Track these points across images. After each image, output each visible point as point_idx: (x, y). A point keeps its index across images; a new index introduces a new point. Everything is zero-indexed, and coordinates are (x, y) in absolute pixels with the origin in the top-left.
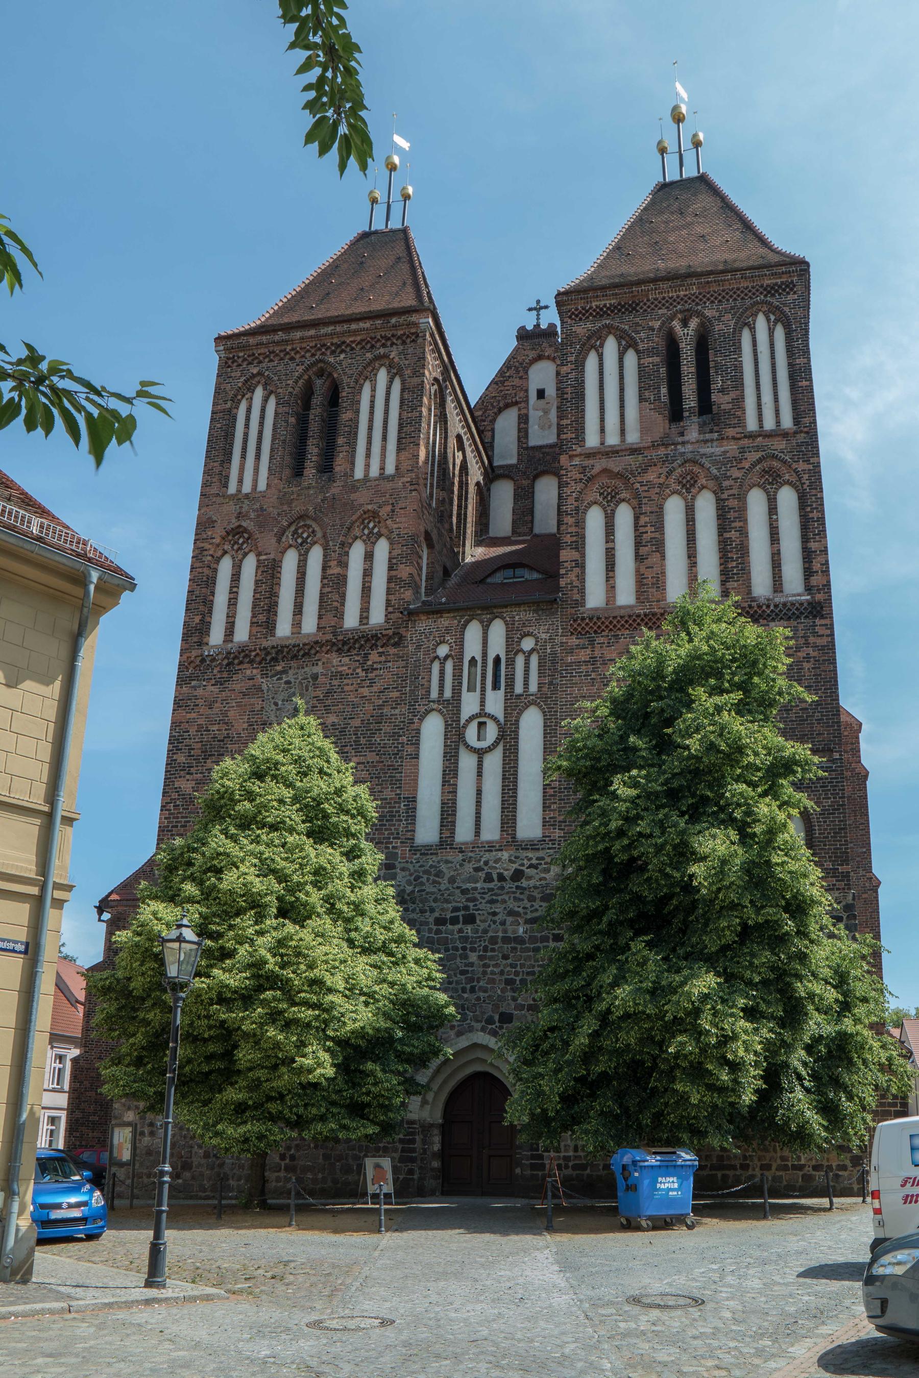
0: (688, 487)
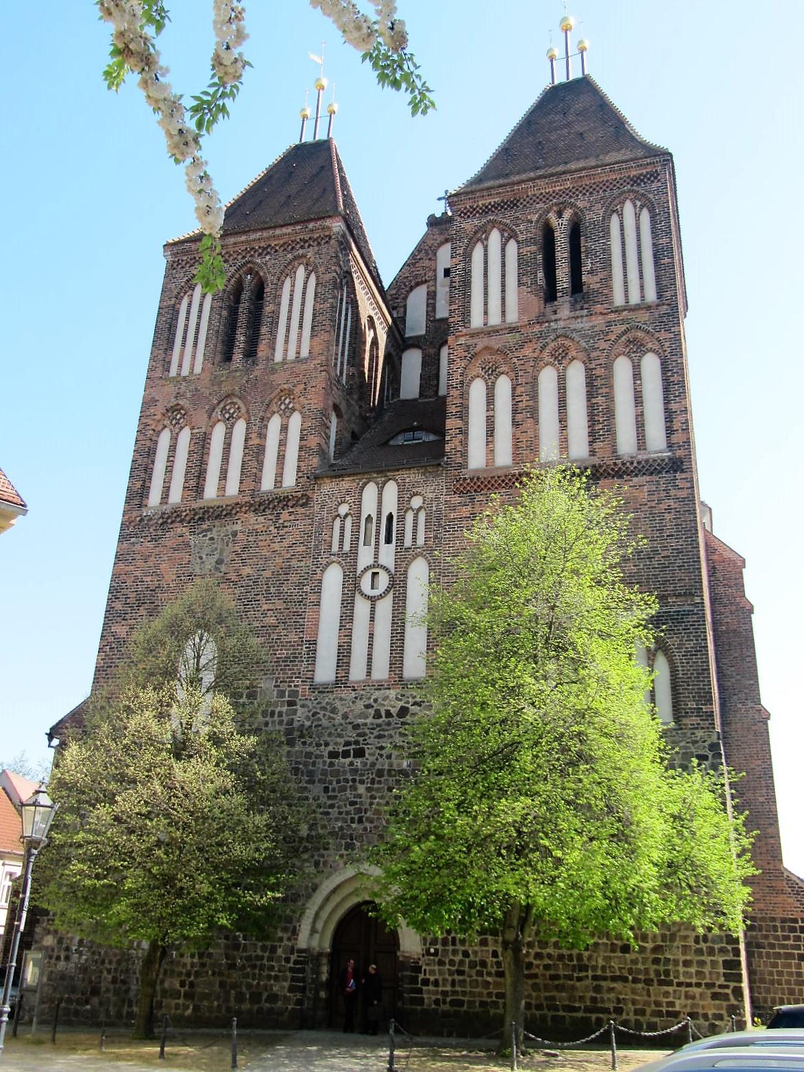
0: (561, 357)
